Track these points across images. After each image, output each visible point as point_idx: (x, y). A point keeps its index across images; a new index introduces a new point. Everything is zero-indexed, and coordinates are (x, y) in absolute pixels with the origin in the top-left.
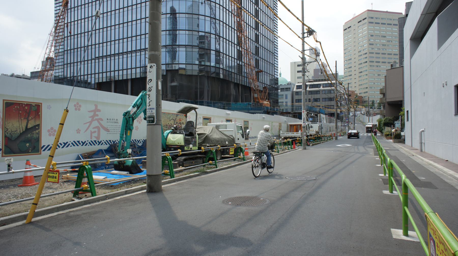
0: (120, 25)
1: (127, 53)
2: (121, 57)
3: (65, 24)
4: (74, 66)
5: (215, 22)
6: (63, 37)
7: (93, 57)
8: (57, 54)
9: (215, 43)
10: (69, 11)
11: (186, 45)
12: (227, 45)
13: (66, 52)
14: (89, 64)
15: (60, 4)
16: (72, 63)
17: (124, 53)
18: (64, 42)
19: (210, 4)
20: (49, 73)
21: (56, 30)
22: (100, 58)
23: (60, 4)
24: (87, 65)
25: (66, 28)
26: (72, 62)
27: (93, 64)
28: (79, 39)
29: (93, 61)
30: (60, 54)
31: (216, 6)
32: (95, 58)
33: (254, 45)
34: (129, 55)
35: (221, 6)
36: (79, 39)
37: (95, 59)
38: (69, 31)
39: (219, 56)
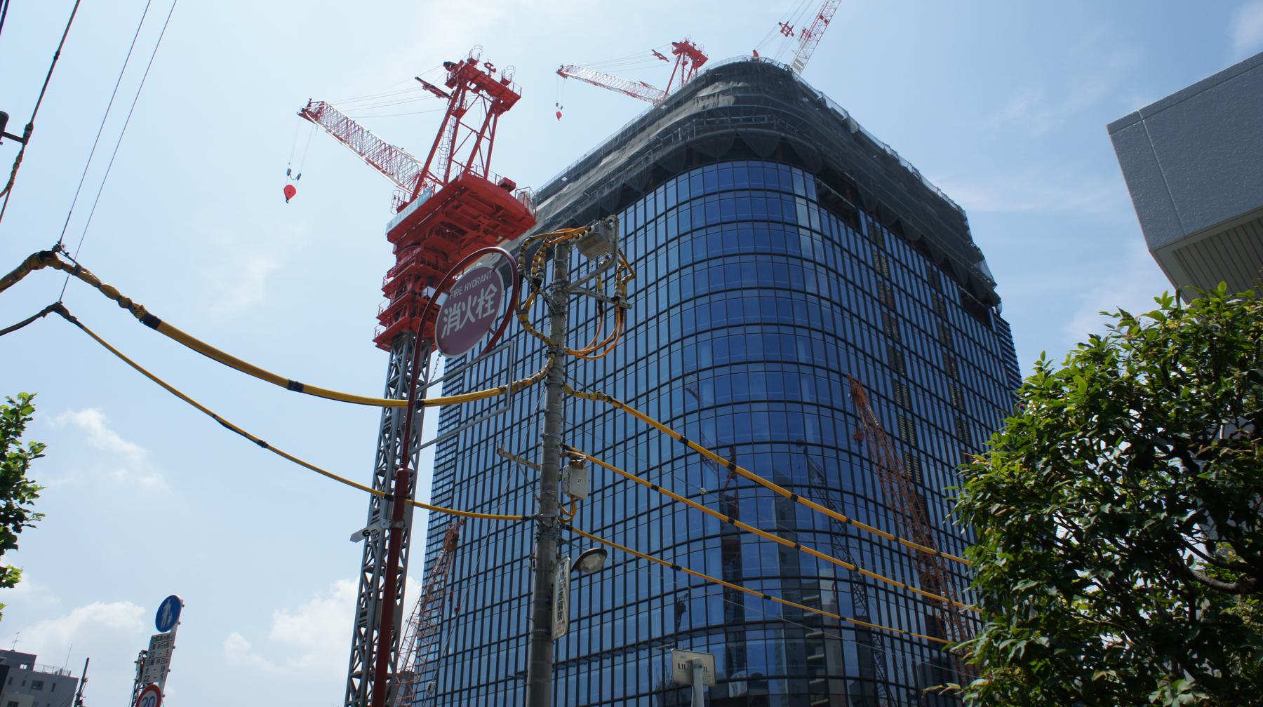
0: (677, 548)
1: (601, 656)
2: (619, 660)
3: (446, 586)
4: (478, 696)
5: (847, 546)
6: (440, 622)
7: (511, 672)
8: (421, 667)
9: (854, 604)
10: (459, 551)
11: (838, 601)
12: (893, 607)
13: (443, 662)
14: (499, 694)
15: (440, 545)
16: (492, 683)
17: (628, 647)
18: (441, 634)
19: (827, 495)
20: (771, 673)
21: (423, 606)
22: (571, 664)
23: (440, 545)
24: (503, 693)
25: (447, 603)
26: (490, 681)
27: (510, 693)
28: (514, 613)
29: (511, 684)
30: (430, 667)
31: (845, 500)
32: (516, 673)
33: (921, 616)
34: (607, 662)
35: (859, 496)
36: (514, 613)
37: (515, 679)
38: (455, 605)
39: (871, 643)
